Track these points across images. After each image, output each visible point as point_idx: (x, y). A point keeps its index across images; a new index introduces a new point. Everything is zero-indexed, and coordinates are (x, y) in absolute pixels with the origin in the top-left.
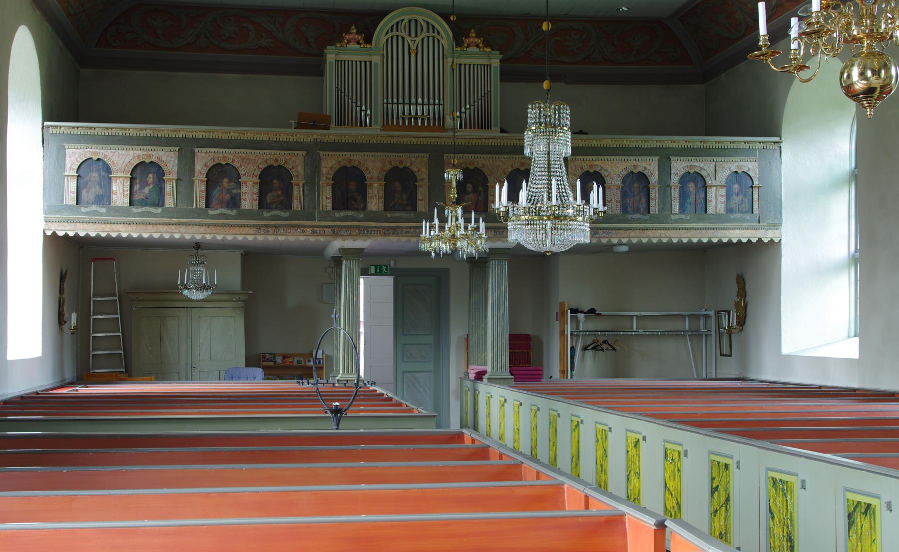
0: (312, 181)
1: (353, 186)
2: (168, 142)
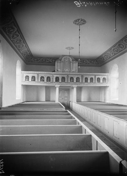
0: (68, 79)
1: (58, 79)
2: (36, 74)
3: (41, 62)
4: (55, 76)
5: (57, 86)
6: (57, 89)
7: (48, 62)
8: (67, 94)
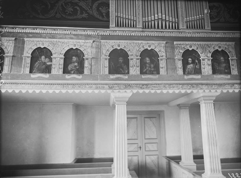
1: (121, 60)
3: (58, 16)
4: (109, 46)
5: (120, 94)
6: (120, 113)
7: (85, 15)
8: (154, 129)
